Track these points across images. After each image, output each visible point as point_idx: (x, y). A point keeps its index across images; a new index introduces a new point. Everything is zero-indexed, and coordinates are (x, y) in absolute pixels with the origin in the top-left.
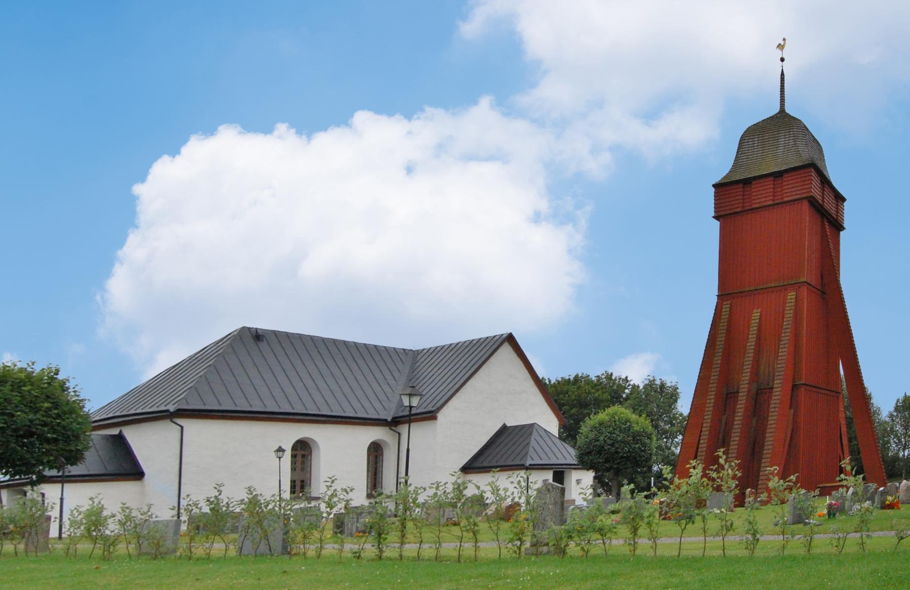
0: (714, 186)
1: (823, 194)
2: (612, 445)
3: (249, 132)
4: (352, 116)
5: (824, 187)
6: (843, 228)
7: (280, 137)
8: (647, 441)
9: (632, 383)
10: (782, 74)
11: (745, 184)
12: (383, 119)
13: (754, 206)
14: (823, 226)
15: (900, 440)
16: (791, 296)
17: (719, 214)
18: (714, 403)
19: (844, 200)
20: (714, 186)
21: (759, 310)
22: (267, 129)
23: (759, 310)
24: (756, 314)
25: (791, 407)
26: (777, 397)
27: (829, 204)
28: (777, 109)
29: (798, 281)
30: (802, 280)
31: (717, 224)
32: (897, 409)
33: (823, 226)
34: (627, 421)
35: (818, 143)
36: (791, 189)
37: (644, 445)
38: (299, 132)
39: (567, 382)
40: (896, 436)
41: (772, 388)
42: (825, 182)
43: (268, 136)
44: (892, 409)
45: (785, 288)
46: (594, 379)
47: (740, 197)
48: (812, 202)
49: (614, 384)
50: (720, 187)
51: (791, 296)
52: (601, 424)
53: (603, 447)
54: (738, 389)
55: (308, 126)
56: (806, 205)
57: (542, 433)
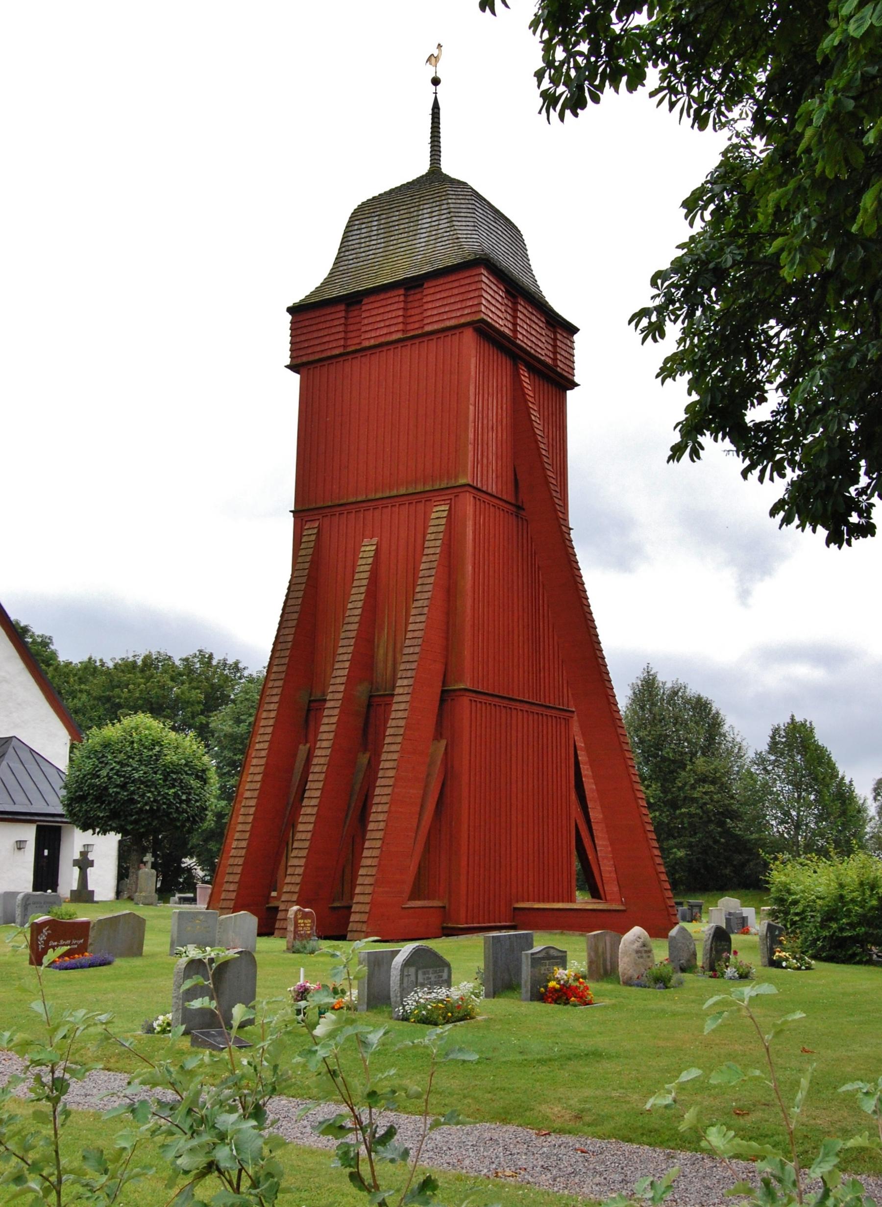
0: (290, 310)
1: (515, 317)
2: (123, 786)
5: (515, 303)
6: (573, 385)
8: (194, 783)
10: (436, 108)
11: (348, 305)
13: (366, 344)
14: (516, 377)
16: (439, 512)
17: (299, 361)
19: (572, 330)
20: (290, 310)
21: (375, 540)
23: (375, 540)
24: (368, 549)
25: (438, 735)
26: (400, 714)
27: (531, 336)
28: (423, 167)
29: (452, 483)
30: (462, 481)
31: (295, 379)
32: (773, 746)
33: (516, 377)
34: (156, 743)
35: (511, 223)
36: (440, 309)
37: (186, 789)
41: (393, 695)
42: (523, 294)
45: (427, 497)
48: (485, 332)
50: (301, 313)
51: (439, 512)
52: (106, 745)
53: (106, 789)
54: (324, 693)
56: (469, 336)
57: (26, 756)
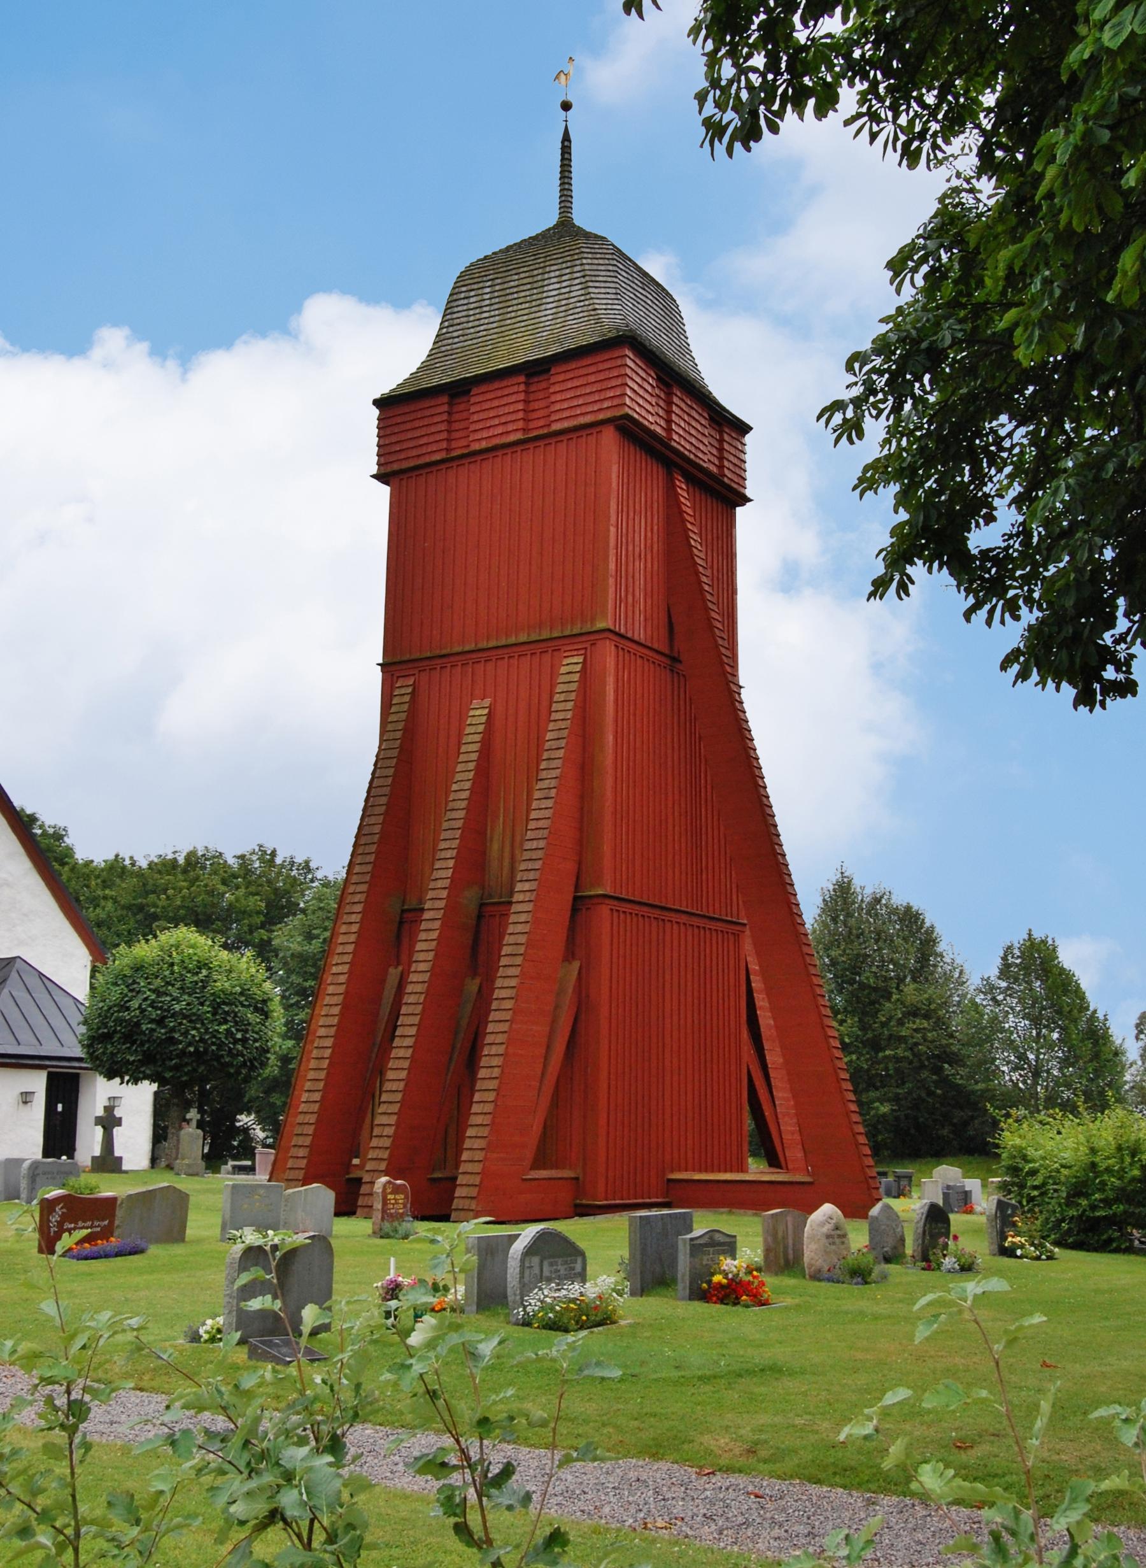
0: (377, 403)
1: (669, 412)
2: (160, 1022)
3: (26, 349)
4: (298, 308)
5: (669, 394)
6: (744, 500)
7: (107, 365)
8: (253, 1017)
9: (319, 875)
11: (452, 396)
12: (382, 315)
13: (476, 447)
14: (671, 489)
15: (1022, 1057)
16: (571, 665)
17: (389, 469)
18: (359, 933)
19: (743, 429)
20: (377, 403)
21: (487, 702)
22: (75, 345)
23: (487, 702)
24: (478, 713)
25: (570, 954)
26: (520, 928)
27: (690, 436)
29: (588, 628)
30: (601, 625)
32: (1005, 970)
33: (671, 489)
34: (203, 965)
36: (571, 401)
37: (242, 1024)
38: (158, 352)
39: (167, 866)
40: (1010, 1044)
42: (677, 382)
43: (77, 362)
44: (993, 972)
45: (555, 646)
46: (231, 861)
47: (443, 427)
48: (630, 431)
49: (279, 873)
50: (392, 406)
51: (571, 665)
52: (138, 968)
53: (138, 1024)
54: (421, 901)
55: (182, 335)
56: (609, 437)
57: (33, 982)
